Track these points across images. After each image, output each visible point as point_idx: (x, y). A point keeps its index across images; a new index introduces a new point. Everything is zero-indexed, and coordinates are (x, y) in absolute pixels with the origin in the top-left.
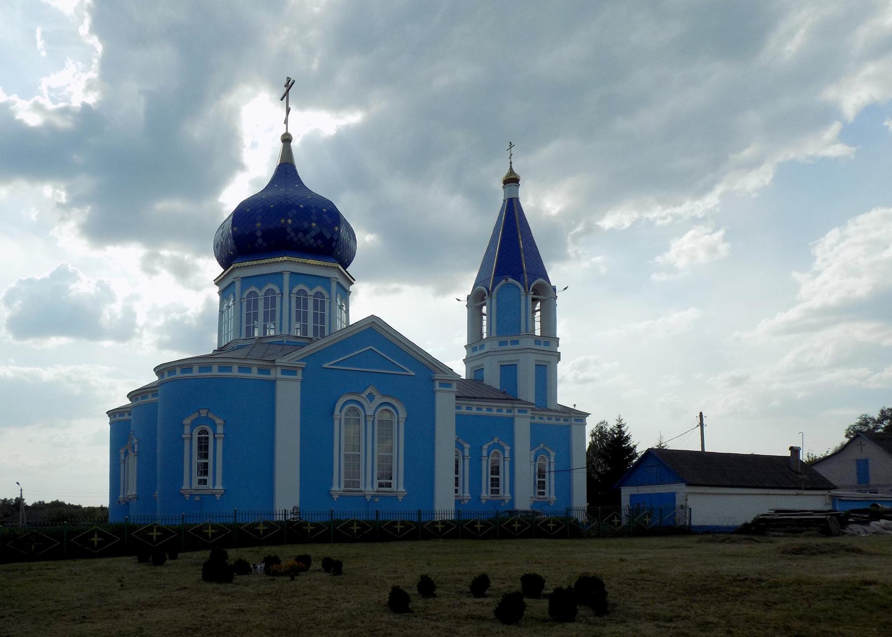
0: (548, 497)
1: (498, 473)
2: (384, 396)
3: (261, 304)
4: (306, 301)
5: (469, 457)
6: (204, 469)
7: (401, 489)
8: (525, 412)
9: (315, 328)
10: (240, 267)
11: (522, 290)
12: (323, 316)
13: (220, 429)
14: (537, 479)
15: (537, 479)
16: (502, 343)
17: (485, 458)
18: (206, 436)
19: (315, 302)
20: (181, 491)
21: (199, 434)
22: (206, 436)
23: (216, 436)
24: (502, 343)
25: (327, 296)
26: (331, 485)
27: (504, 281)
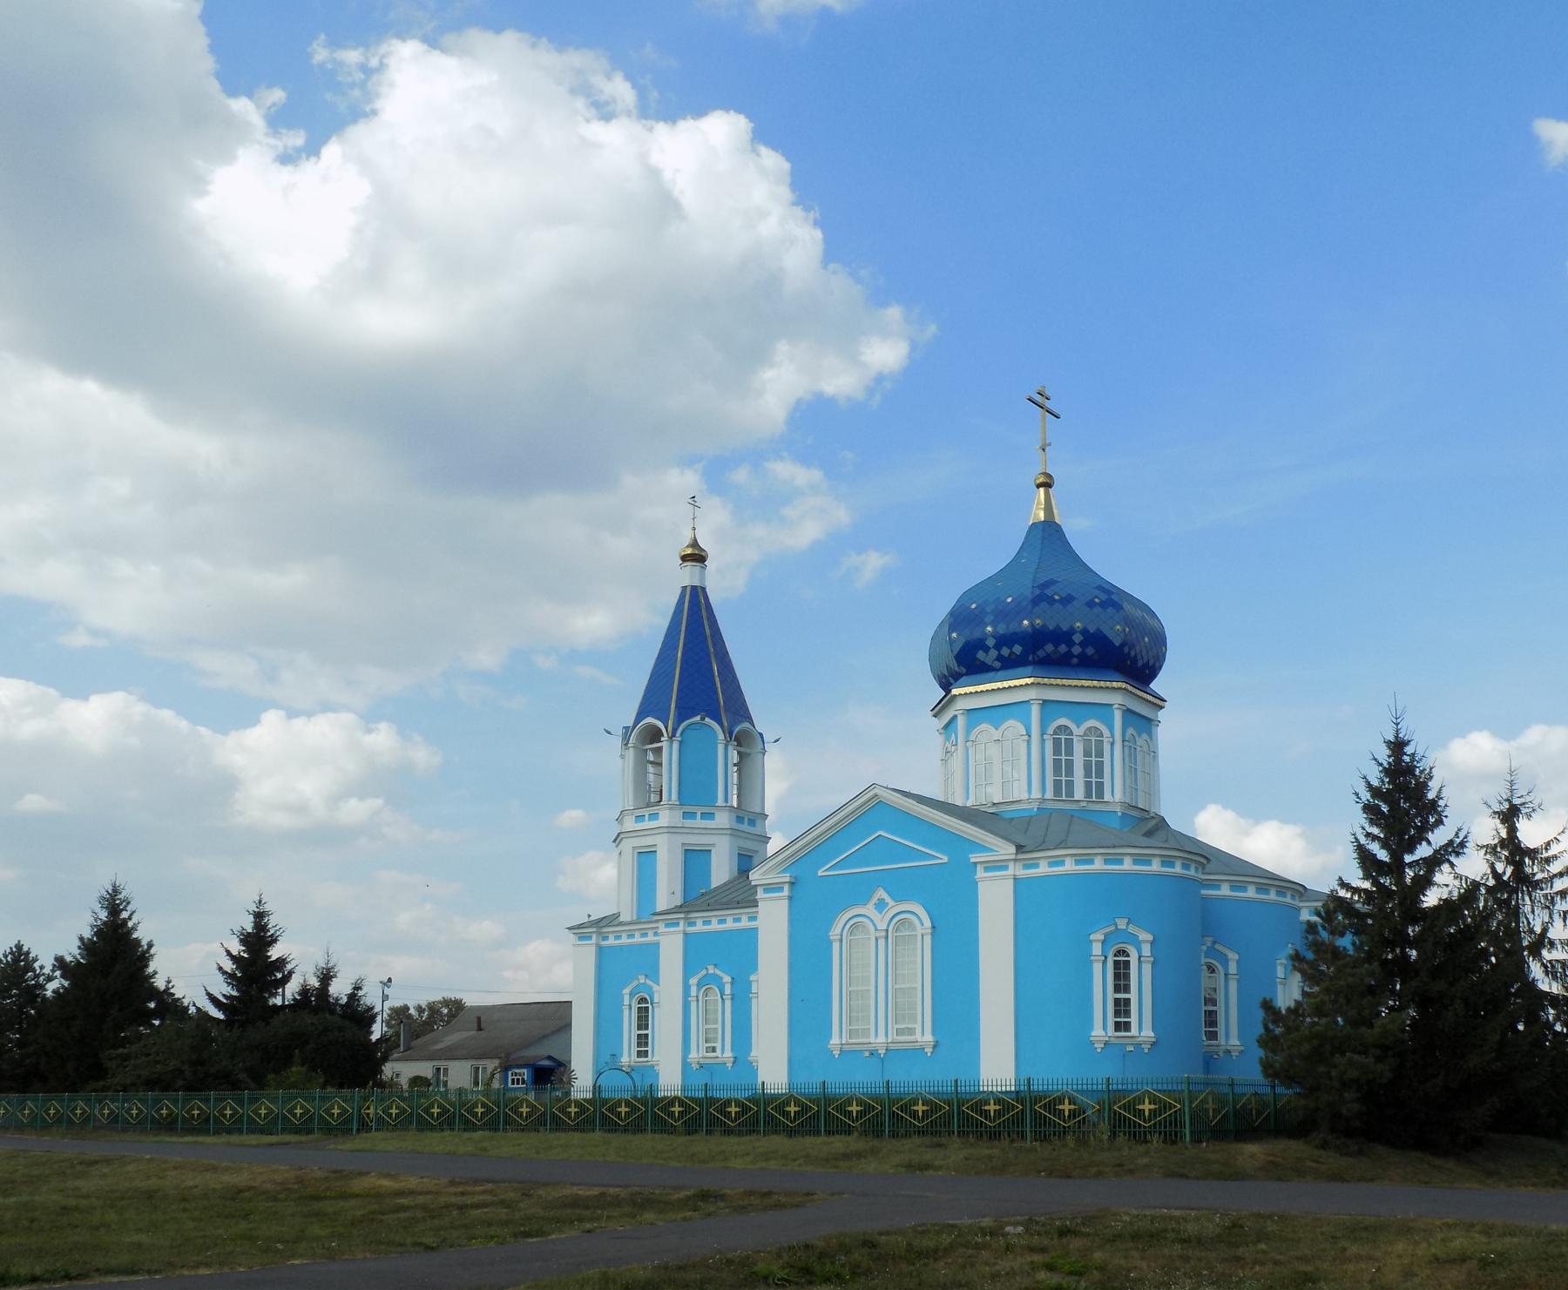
0: (720, 1056)
1: (1117, 1002)
2: (898, 901)
3: (1078, 748)
4: (1069, 743)
5: (1237, 977)
6: (1122, 1007)
7: (1148, 1033)
8: (590, 938)
9: (1088, 785)
10: (987, 691)
11: (721, 736)
12: (1100, 765)
13: (1233, 969)
14: (649, 1032)
15: (649, 1032)
16: (686, 815)
17: (1234, 977)
18: (1126, 959)
19: (1087, 743)
20: (1092, 1039)
21: (1115, 955)
22: (1126, 959)
23: (1142, 959)
24: (686, 815)
25: (1106, 733)
26: (1091, 1028)
27: (698, 718)
